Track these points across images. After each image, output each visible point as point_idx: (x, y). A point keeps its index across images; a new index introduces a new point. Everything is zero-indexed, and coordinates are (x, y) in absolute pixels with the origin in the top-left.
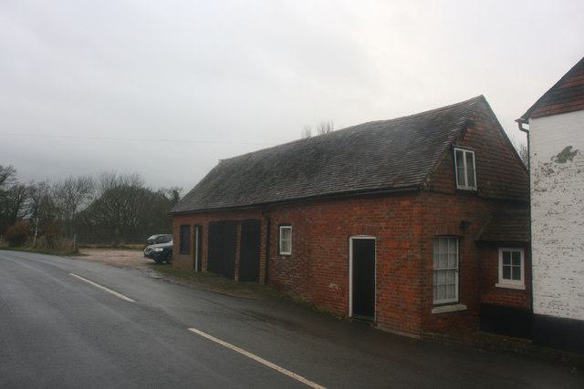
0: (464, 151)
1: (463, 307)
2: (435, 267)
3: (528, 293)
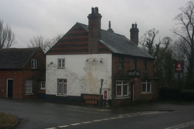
0: (34, 60)
1: (33, 94)
2: (26, 85)
3: (45, 90)
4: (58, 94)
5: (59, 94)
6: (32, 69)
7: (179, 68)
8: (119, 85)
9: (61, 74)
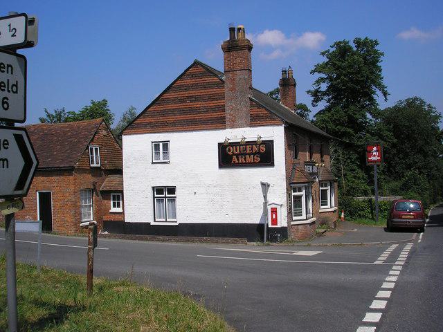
4: (155, 221)
5: (294, 218)
6: (226, 151)
7: (375, 156)
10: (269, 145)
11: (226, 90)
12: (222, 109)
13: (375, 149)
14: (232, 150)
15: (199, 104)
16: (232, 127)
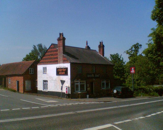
4: (44, 90)
5: (44, 90)
8: (103, 82)
9: (45, 77)
10: (67, 69)
11: (58, 52)
12: (57, 58)
13: (133, 68)
14: (60, 70)
15: (52, 57)
16: (59, 63)
